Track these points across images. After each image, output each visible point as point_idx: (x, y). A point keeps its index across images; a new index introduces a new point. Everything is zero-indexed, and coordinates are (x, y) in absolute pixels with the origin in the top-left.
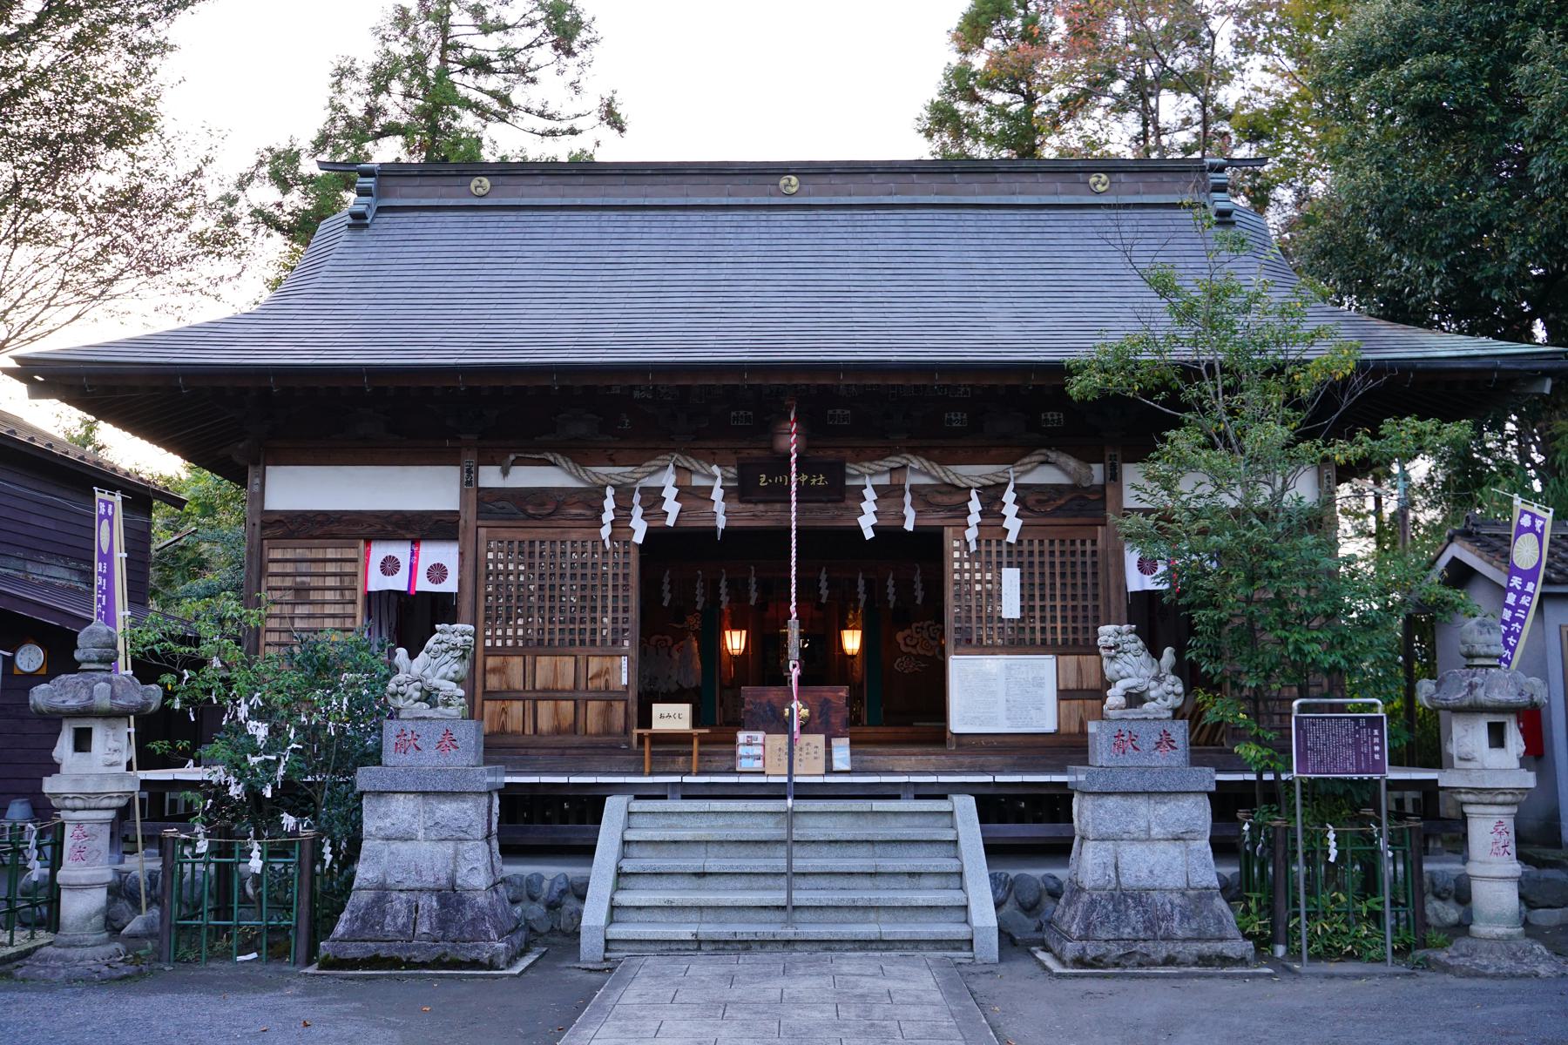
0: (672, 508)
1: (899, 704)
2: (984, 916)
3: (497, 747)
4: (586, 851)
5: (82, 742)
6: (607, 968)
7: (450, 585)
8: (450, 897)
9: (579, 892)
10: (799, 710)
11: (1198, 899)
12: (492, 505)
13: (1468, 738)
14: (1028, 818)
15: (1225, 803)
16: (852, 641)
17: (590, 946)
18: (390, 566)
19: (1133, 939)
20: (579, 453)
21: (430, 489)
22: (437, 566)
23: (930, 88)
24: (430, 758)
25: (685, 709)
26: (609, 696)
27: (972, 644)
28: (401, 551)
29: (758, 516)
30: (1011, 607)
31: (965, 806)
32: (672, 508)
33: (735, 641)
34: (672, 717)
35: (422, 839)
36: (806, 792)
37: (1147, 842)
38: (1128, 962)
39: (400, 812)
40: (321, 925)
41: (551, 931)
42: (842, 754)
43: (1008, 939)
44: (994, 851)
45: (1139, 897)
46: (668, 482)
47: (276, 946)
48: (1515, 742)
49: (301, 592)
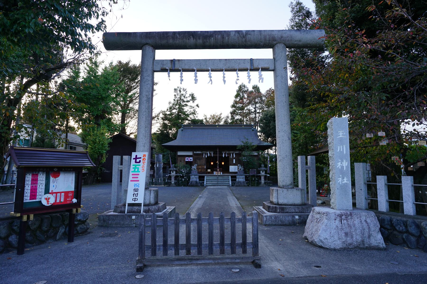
0: (209, 155)
1: (225, 169)
2: (231, 183)
3: (199, 173)
4: (204, 180)
5: (173, 172)
6: (206, 187)
7: (192, 160)
8: (196, 182)
9: (204, 183)
10: (218, 170)
11: (244, 182)
12: (195, 154)
13: (261, 172)
14: (234, 178)
15: (246, 176)
16: (223, 163)
17: (205, 185)
18: (187, 159)
19: (240, 185)
20: (201, 151)
21: (190, 153)
22: (191, 159)
23: (232, 103)
24: (194, 173)
25: (115, 157)
26: (204, 169)
27: (231, 165)
28: (188, 158)
29: (215, 155)
30: (234, 162)
31: (230, 177)
32: (209, 155)
33: (212, 163)
34: (209, 170)
35: (194, 178)
36: (219, 176)
37: (241, 179)
38: (239, 186)
39: (193, 176)
40: (188, 183)
41: (202, 185)
42: (221, 173)
43: (232, 186)
44: (232, 180)
45: (240, 182)
46: (208, 153)
47: (185, 186)
48: (264, 172)
49: (181, 161)
